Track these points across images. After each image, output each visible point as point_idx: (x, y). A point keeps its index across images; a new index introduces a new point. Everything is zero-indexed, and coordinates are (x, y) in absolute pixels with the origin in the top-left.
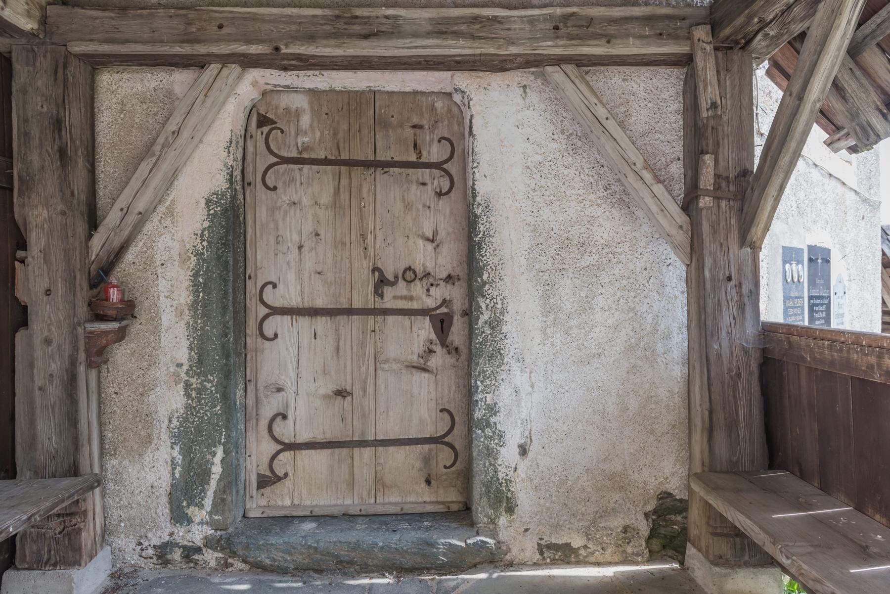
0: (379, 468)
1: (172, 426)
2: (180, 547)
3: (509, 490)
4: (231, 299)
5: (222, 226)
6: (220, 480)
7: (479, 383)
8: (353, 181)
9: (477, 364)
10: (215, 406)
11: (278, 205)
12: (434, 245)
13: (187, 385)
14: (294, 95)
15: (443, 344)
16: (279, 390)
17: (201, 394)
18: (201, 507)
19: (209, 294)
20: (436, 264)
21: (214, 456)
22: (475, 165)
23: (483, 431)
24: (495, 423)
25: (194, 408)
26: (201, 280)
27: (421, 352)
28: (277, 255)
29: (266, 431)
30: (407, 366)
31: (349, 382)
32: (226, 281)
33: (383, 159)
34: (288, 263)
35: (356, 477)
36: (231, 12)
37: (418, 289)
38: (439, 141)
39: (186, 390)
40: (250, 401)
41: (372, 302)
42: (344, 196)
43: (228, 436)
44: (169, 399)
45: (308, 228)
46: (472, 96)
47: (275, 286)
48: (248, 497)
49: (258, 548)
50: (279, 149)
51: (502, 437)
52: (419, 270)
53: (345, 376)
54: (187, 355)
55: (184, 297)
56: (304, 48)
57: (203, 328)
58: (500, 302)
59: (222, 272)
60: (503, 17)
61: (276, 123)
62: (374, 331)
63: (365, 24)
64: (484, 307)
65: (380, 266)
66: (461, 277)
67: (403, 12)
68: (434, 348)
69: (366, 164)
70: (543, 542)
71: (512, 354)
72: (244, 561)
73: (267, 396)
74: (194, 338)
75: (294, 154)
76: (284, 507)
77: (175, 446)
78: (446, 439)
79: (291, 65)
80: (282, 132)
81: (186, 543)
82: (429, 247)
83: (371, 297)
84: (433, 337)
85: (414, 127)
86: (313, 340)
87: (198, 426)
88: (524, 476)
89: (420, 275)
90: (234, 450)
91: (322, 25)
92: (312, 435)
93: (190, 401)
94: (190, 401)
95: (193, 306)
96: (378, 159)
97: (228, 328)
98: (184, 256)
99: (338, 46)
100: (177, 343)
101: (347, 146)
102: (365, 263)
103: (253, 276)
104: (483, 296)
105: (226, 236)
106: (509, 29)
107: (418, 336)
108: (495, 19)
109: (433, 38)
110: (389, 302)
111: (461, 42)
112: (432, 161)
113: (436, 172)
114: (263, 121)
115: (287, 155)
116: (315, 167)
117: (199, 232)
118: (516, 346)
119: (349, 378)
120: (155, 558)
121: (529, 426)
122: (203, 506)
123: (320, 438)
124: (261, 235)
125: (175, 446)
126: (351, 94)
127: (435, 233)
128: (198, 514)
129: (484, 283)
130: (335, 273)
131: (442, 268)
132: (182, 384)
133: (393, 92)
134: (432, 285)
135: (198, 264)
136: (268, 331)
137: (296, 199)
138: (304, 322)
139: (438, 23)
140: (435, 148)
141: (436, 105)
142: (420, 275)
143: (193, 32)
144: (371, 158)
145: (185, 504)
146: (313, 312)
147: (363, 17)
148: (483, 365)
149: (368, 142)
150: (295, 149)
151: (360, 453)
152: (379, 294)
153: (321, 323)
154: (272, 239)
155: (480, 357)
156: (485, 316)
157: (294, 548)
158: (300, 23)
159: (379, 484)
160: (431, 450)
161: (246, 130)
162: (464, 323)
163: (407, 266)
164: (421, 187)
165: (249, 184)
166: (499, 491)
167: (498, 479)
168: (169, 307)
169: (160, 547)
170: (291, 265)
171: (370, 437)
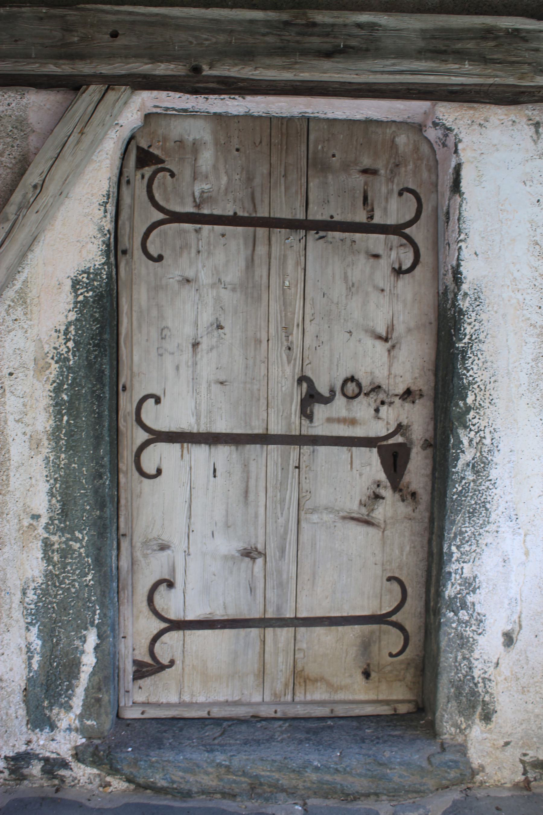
0: (299, 655)
1: (27, 600)
2: (40, 760)
3: (487, 692)
4: (106, 424)
5: (96, 320)
6: (93, 674)
7: (454, 548)
8: (273, 249)
9: (453, 523)
10: (86, 575)
11: (164, 282)
12: (389, 345)
13: (47, 545)
14: (191, 121)
15: (396, 487)
16: (163, 547)
17: (66, 558)
18: (69, 708)
19: (77, 417)
20: (390, 374)
21: (85, 642)
22: (462, 237)
23: (456, 614)
24: (473, 604)
25: (57, 576)
26: (65, 398)
27: (364, 498)
28: (161, 355)
29: (145, 603)
30: (344, 518)
31: (261, 539)
32: (99, 399)
33: (319, 217)
34: (177, 368)
35: (267, 666)
36: (130, 13)
37: (363, 408)
38: (400, 194)
39: (45, 552)
40: (124, 563)
41: (296, 425)
42: (261, 271)
43: (103, 616)
44: (22, 564)
45: (207, 317)
46: (461, 136)
47: (158, 401)
48: (122, 691)
49: (152, 766)
50: (168, 201)
51: (481, 621)
52: (365, 383)
53: (256, 529)
54: (46, 504)
55: (42, 421)
56: (236, 69)
57: (67, 466)
58: (488, 436)
59: (94, 386)
60: (528, 31)
61: (163, 162)
62: (298, 467)
63: (327, 35)
64: (465, 441)
65: (309, 374)
66: (425, 393)
67: (383, 19)
68: (382, 492)
69: (292, 225)
70: (526, 759)
71: (501, 509)
72: (129, 780)
73: (145, 556)
74: (56, 480)
75: (190, 209)
76: (169, 705)
77: (31, 628)
78: (394, 618)
79: (206, 88)
80: (173, 175)
81: (48, 754)
82: (381, 347)
83: (295, 418)
84: (382, 476)
85: (365, 171)
86: (212, 478)
87: (62, 601)
88: (508, 673)
89: (365, 390)
90: (110, 632)
91: (264, 35)
92: (208, 610)
93: (51, 567)
94: (51, 567)
95: (53, 434)
96: (310, 217)
97: (102, 466)
98: (41, 363)
99: (284, 68)
100: (31, 486)
101: (266, 196)
102: (288, 370)
103: (128, 386)
104: (466, 427)
105: (101, 334)
106: (537, 50)
107: (361, 475)
108: (515, 34)
109: (426, 59)
110: (319, 427)
111: (467, 66)
112: (389, 222)
113: (394, 239)
114: (145, 158)
115: (178, 209)
116: (219, 229)
117: (63, 328)
118: (508, 498)
119: (261, 532)
120: (7, 772)
121: (518, 608)
122: (71, 707)
123: (219, 614)
124: (140, 326)
125: (31, 628)
126: (274, 122)
127: (391, 328)
128: (66, 719)
129: (468, 409)
130: (245, 383)
131: (399, 380)
132: (40, 543)
133: (335, 120)
134: (383, 403)
135: (61, 373)
136: (149, 467)
137: (190, 274)
138: (200, 452)
139: (433, 38)
140: (394, 203)
141: (397, 140)
142: (365, 390)
143: (73, 43)
144: (301, 216)
145: (46, 703)
146: (212, 439)
147: (324, 25)
148: (459, 524)
149: (297, 192)
150: (191, 199)
151: (275, 635)
152: (306, 413)
153: (223, 452)
154: (154, 334)
155: (457, 512)
156: (467, 456)
157: (198, 766)
158: (232, 31)
159: (299, 677)
160: (372, 632)
161: (121, 173)
162: (426, 458)
163: (349, 375)
164: (372, 260)
165: (124, 252)
166: (474, 693)
167: (473, 678)
168: (20, 434)
169: (13, 759)
170: (181, 371)
171: (289, 614)
